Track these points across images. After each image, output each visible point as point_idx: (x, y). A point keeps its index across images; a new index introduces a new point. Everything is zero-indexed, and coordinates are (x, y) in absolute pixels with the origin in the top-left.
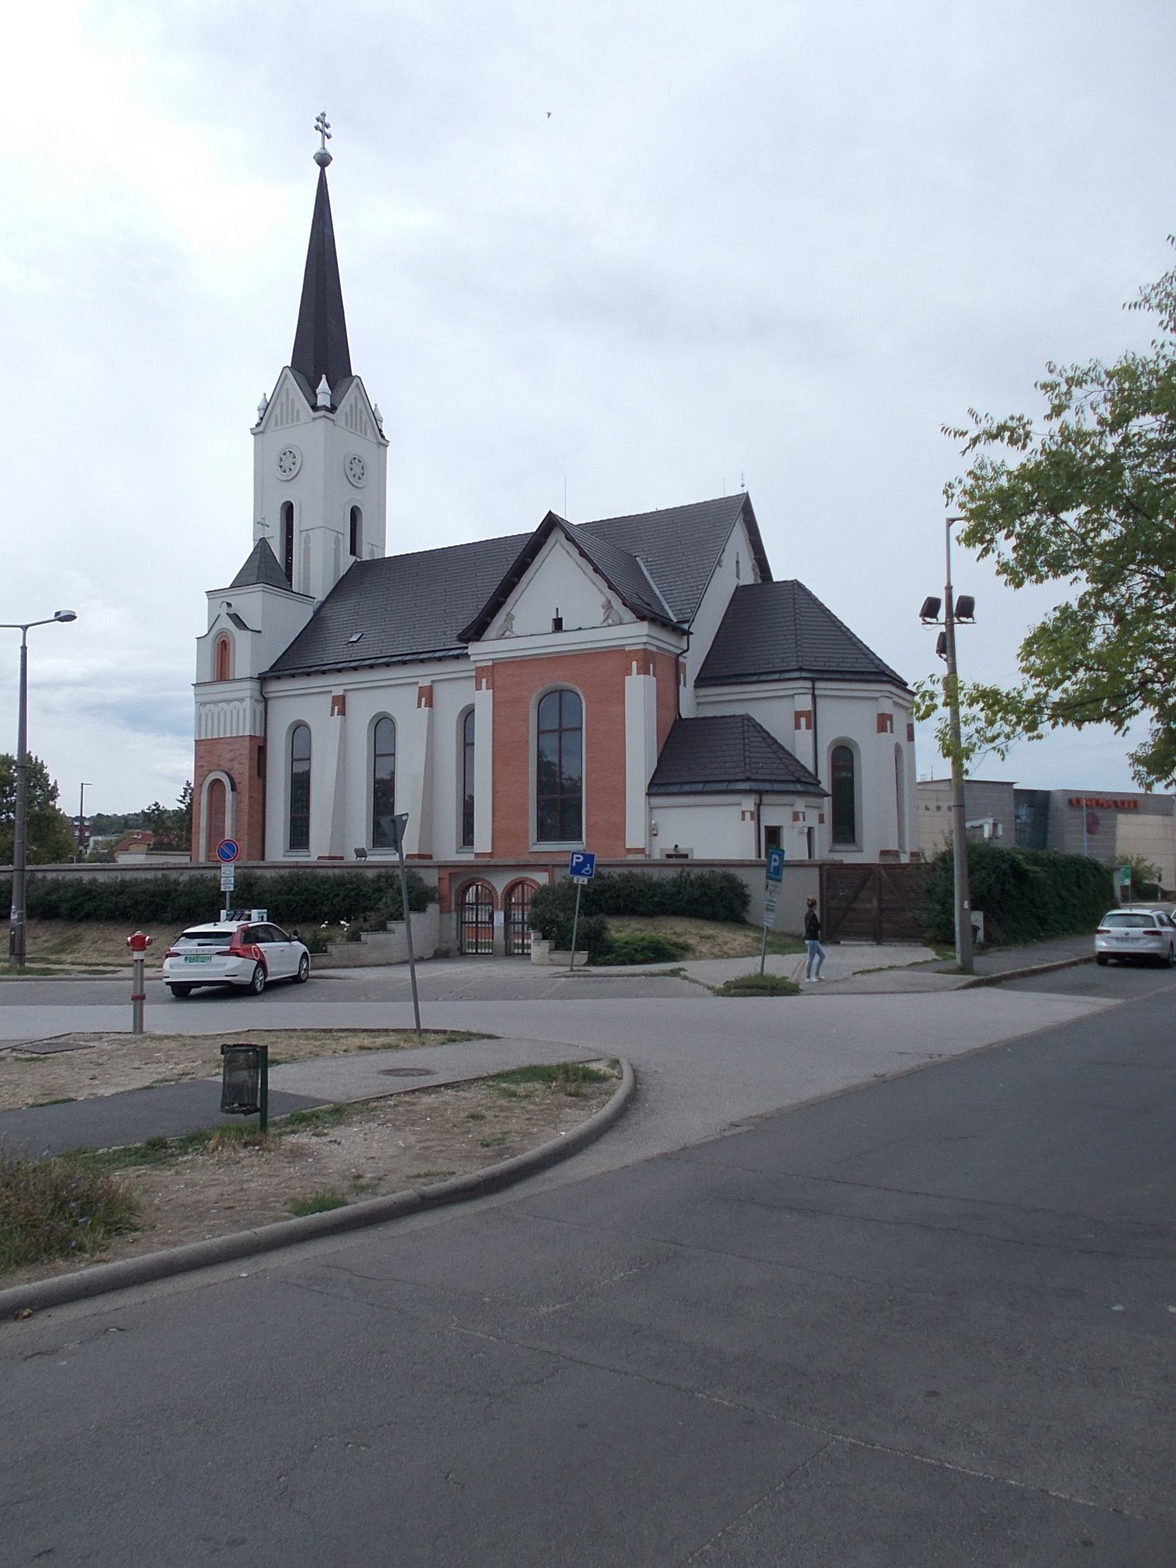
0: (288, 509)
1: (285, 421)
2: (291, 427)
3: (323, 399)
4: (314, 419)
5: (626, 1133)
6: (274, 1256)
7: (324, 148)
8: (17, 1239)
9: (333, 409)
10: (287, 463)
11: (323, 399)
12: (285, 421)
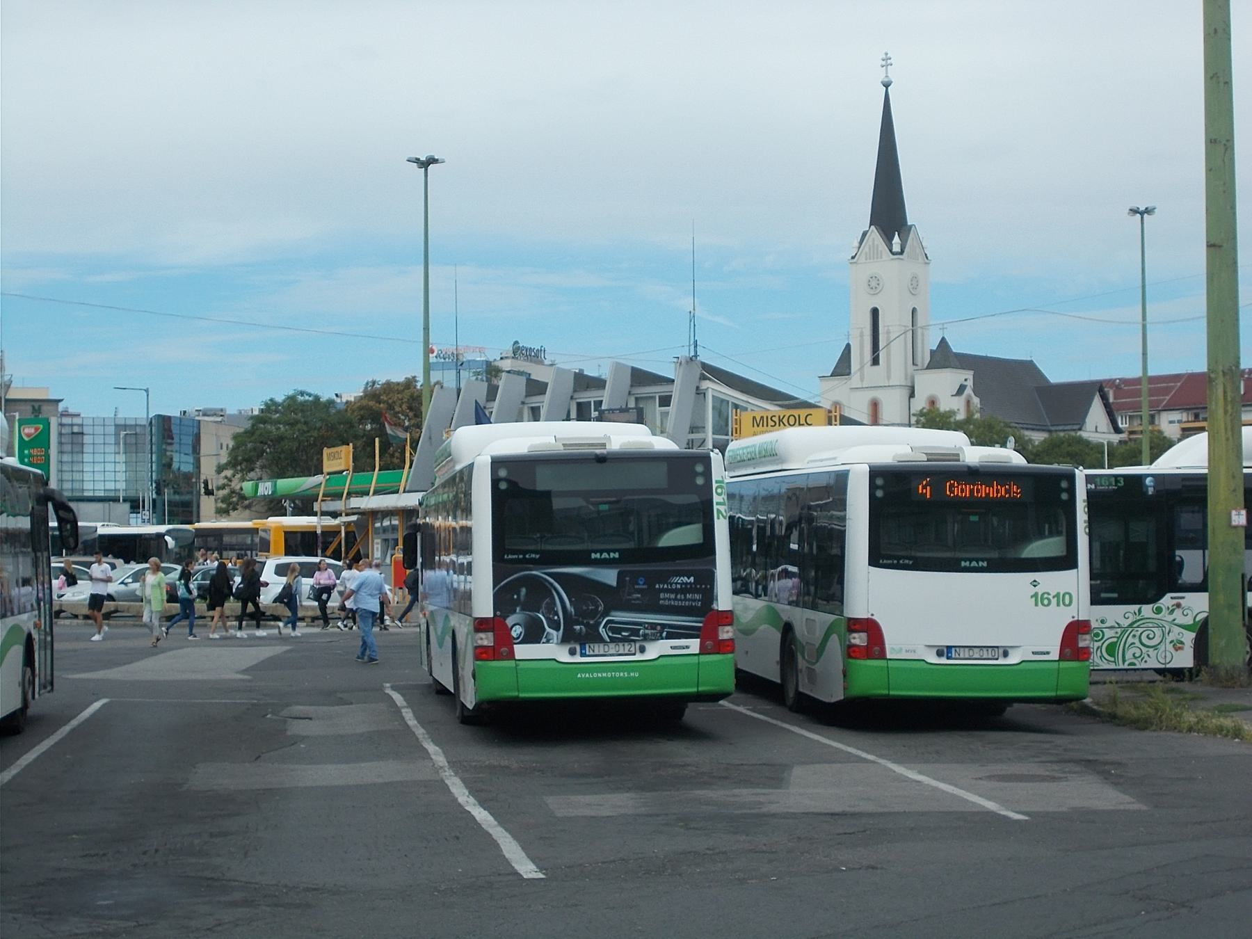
0: (875, 312)
1: (875, 256)
2: (869, 263)
3: (896, 248)
4: (892, 259)
5: (87, 439)
6: (801, 718)
7: (887, 76)
8: (1176, 711)
9: (902, 252)
10: (873, 284)
11: (896, 248)
12: (875, 256)
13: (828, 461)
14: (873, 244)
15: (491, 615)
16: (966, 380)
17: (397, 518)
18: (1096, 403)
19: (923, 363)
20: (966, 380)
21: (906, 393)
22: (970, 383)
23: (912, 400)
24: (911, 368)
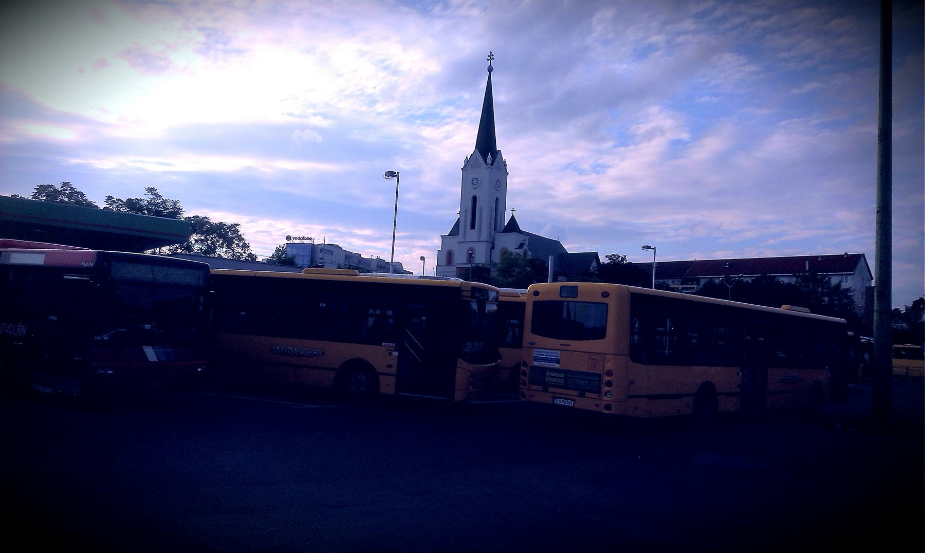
0: (475, 199)
3: (489, 161)
9: (492, 165)
11: (489, 161)
13: (181, 272)
14: (476, 159)
15: (393, 393)
16: (524, 240)
17: (894, 374)
18: (862, 257)
19: (500, 229)
20: (524, 240)
21: (490, 246)
22: (526, 242)
23: (492, 250)
24: (493, 232)
